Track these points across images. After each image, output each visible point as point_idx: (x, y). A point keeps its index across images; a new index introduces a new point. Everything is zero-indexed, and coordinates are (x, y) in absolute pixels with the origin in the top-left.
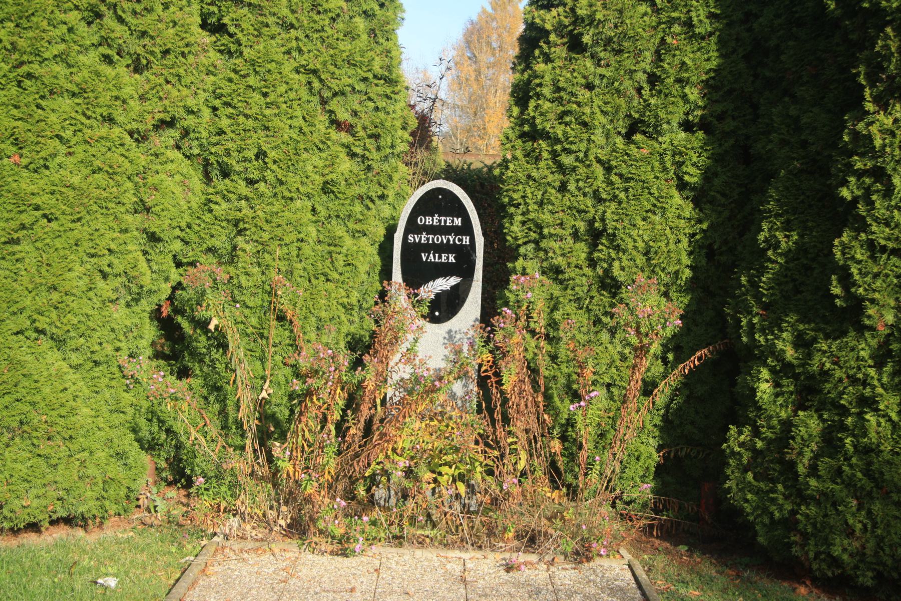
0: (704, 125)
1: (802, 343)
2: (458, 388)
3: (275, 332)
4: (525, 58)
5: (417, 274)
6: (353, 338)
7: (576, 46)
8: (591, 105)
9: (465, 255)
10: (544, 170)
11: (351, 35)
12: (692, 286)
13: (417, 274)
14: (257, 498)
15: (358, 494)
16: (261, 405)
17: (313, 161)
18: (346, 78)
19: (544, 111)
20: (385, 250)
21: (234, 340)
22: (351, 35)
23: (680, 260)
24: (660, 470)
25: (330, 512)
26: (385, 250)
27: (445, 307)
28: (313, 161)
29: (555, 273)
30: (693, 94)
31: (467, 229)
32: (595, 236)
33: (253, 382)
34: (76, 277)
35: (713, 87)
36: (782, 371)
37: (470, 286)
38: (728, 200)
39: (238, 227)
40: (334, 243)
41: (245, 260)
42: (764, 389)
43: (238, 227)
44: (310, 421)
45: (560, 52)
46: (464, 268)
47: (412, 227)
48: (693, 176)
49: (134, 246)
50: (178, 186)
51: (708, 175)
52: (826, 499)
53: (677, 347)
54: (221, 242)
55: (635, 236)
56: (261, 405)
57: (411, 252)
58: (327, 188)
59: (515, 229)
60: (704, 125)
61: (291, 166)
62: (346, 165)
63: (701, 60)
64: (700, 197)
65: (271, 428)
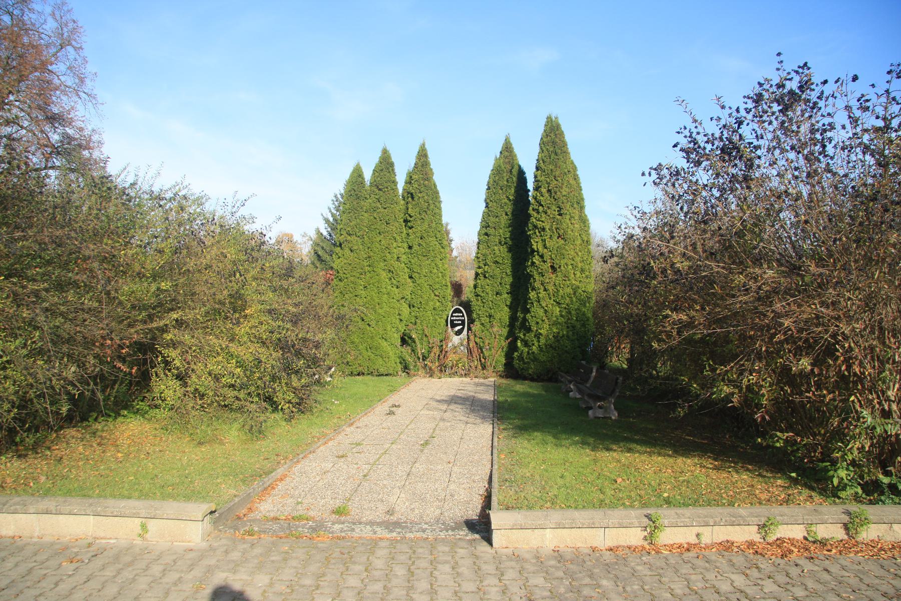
0: (510, 293)
1: (524, 335)
2: (462, 348)
3: (425, 339)
4: (476, 279)
5: (453, 325)
6: (344, 508)
7: (485, 277)
8: (488, 289)
9: (463, 321)
10: (479, 303)
11: (438, 277)
12: (509, 326)
13: (453, 325)
14: (421, 372)
15: (443, 368)
16: (422, 353)
17: (431, 303)
18: (437, 286)
19: (479, 290)
20: (447, 321)
21: (417, 340)
22: (438, 277)
23: (507, 320)
24: (505, 364)
25: (437, 373)
26: (447, 321)
27: (459, 333)
28: (431, 303)
29: (482, 324)
30: (508, 287)
31: (463, 316)
32: (490, 316)
33: (421, 349)
34: (389, 328)
35: (512, 285)
36: (522, 340)
37: (682, 448)
38: (513, 307)
39: (416, 317)
40: (436, 320)
41: (418, 324)
42: (519, 344)
43: (416, 317)
44: (432, 354)
45: (482, 278)
46: (463, 324)
47: (452, 316)
48: (508, 303)
49: (398, 321)
50: (406, 310)
51: (511, 303)
52: (529, 363)
53: (507, 338)
54: (413, 321)
55: (498, 316)
56: (422, 353)
57: (452, 321)
58: (434, 309)
59: (474, 316)
60: (510, 293)
61: (427, 304)
62: (438, 304)
63: (509, 280)
64: (510, 307)
65: (424, 358)
